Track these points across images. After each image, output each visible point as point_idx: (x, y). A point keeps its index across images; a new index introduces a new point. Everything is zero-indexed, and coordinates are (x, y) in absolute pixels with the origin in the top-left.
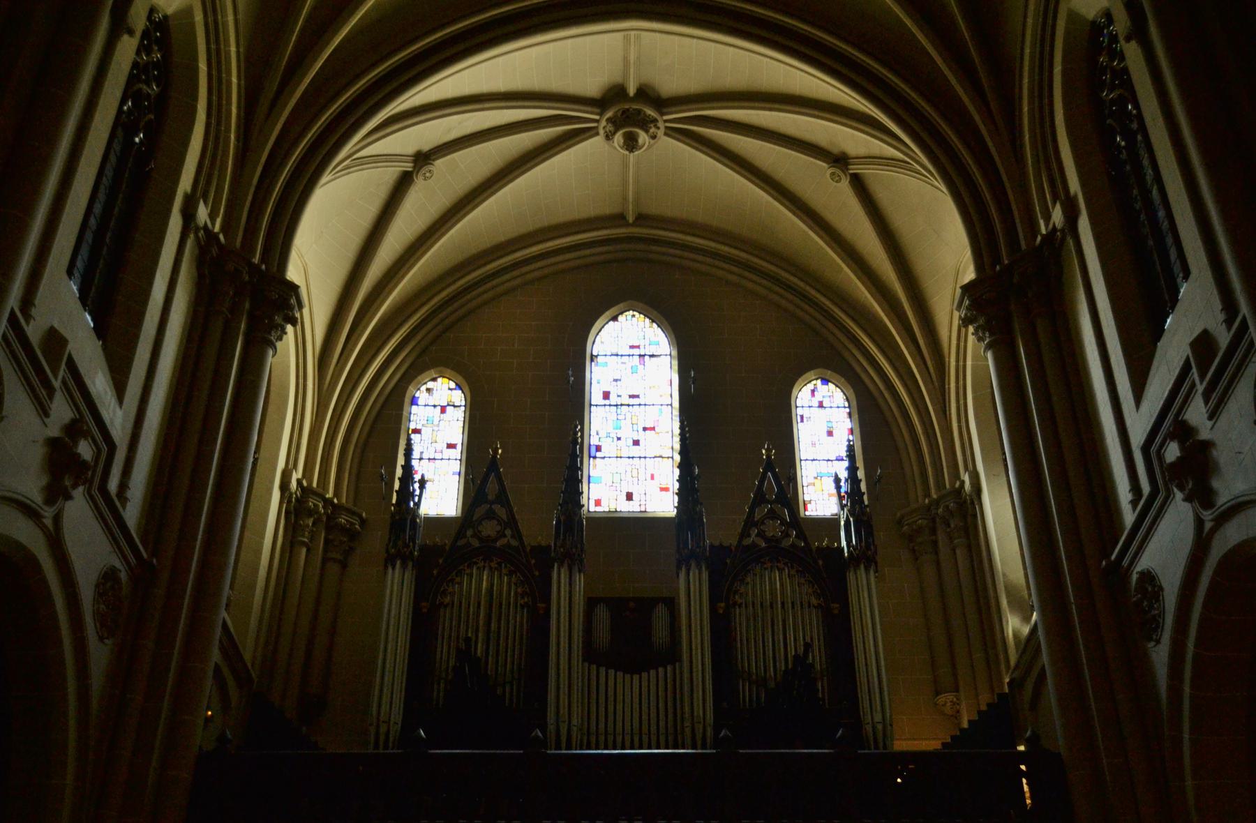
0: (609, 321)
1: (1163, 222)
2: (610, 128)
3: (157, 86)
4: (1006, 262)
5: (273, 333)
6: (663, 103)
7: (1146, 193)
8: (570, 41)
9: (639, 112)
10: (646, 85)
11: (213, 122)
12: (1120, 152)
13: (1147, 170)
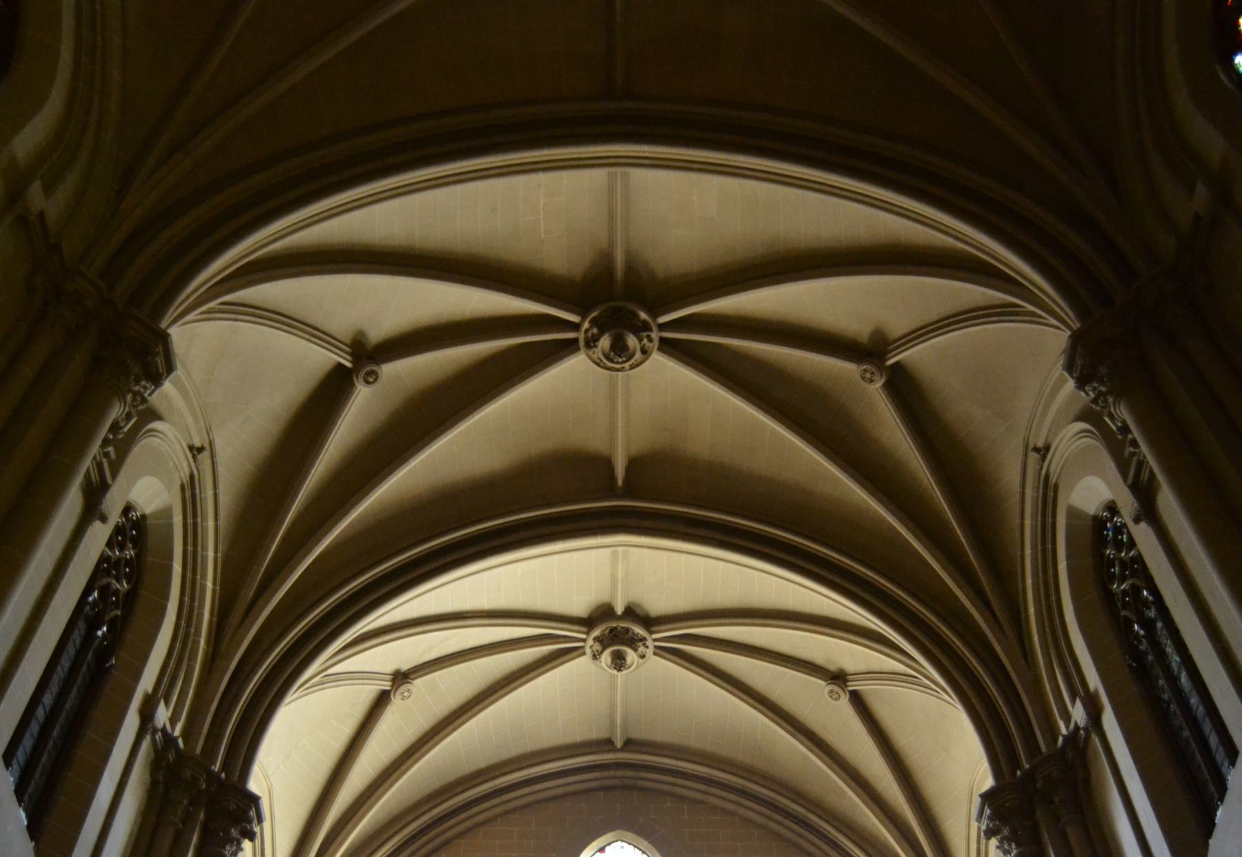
0: (596, 852)
1: (1197, 708)
2: (598, 647)
3: (127, 583)
4: (1027, 766)
5: (228, 848)
6: (650, 622)
7: (1173, 680)
8: (556, 557)
9: (627, 630)
10: (634, 604)
11: (183, 623)
12: (1140, 642)
13: (1172, 657)
